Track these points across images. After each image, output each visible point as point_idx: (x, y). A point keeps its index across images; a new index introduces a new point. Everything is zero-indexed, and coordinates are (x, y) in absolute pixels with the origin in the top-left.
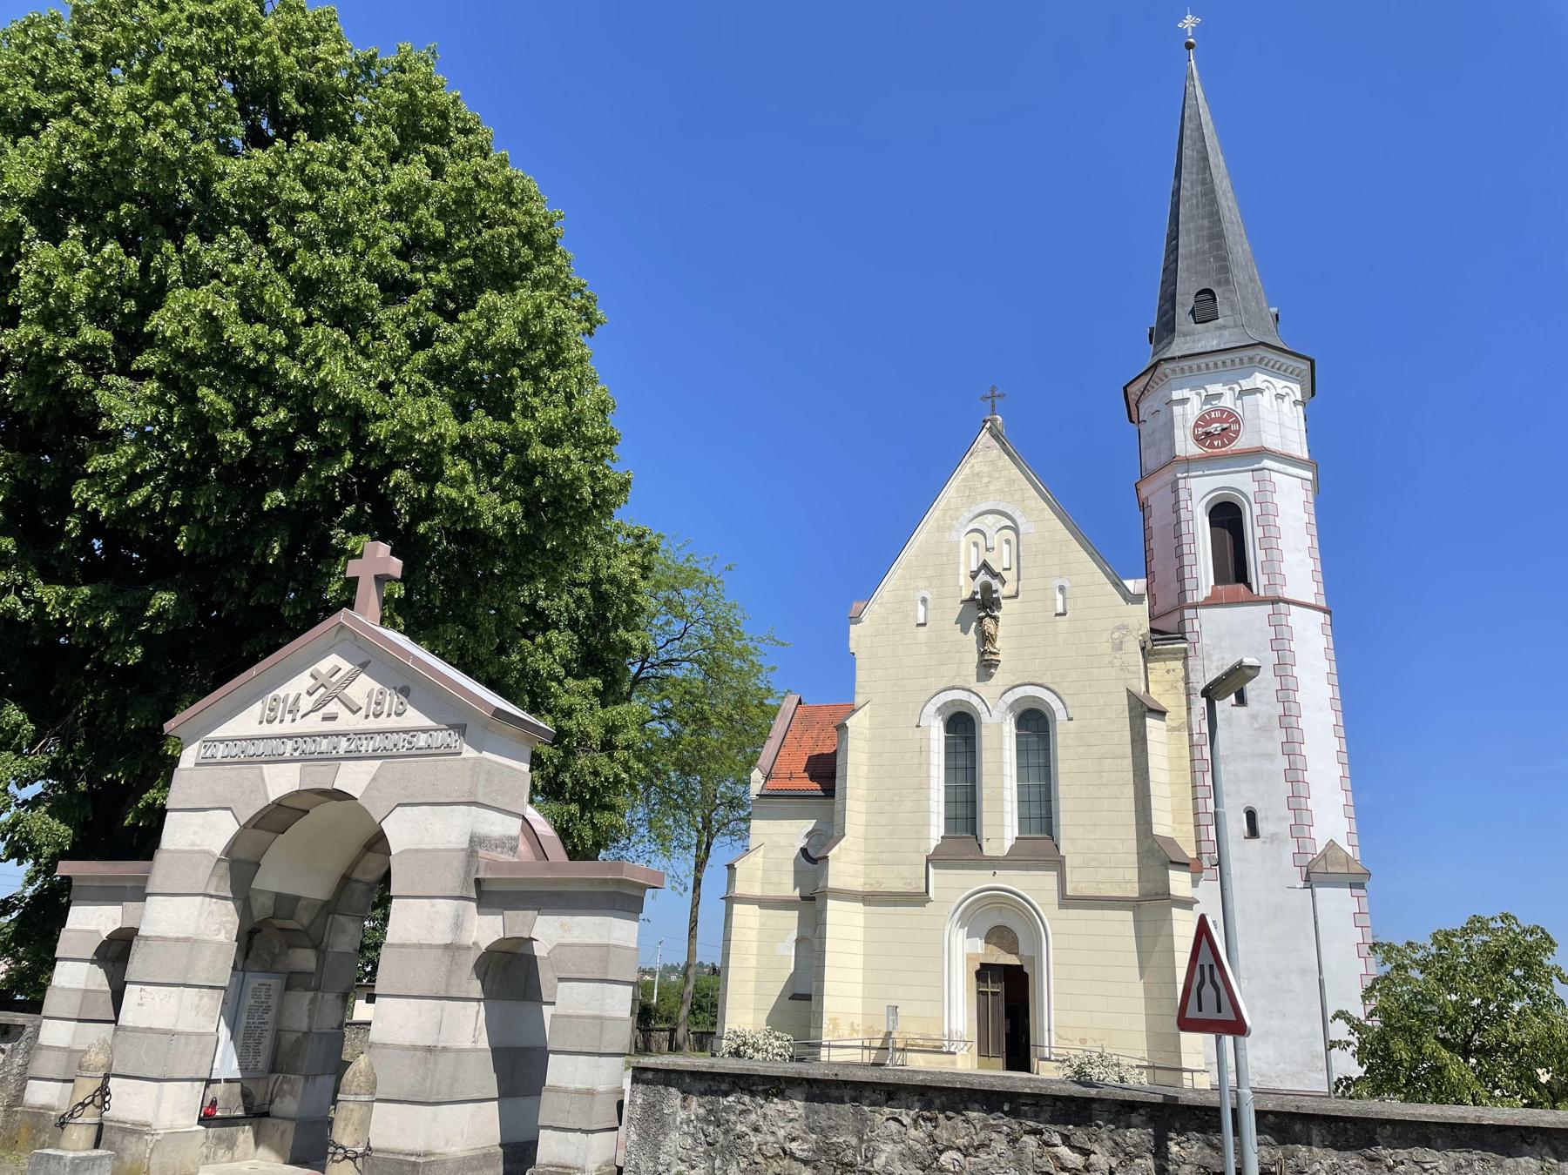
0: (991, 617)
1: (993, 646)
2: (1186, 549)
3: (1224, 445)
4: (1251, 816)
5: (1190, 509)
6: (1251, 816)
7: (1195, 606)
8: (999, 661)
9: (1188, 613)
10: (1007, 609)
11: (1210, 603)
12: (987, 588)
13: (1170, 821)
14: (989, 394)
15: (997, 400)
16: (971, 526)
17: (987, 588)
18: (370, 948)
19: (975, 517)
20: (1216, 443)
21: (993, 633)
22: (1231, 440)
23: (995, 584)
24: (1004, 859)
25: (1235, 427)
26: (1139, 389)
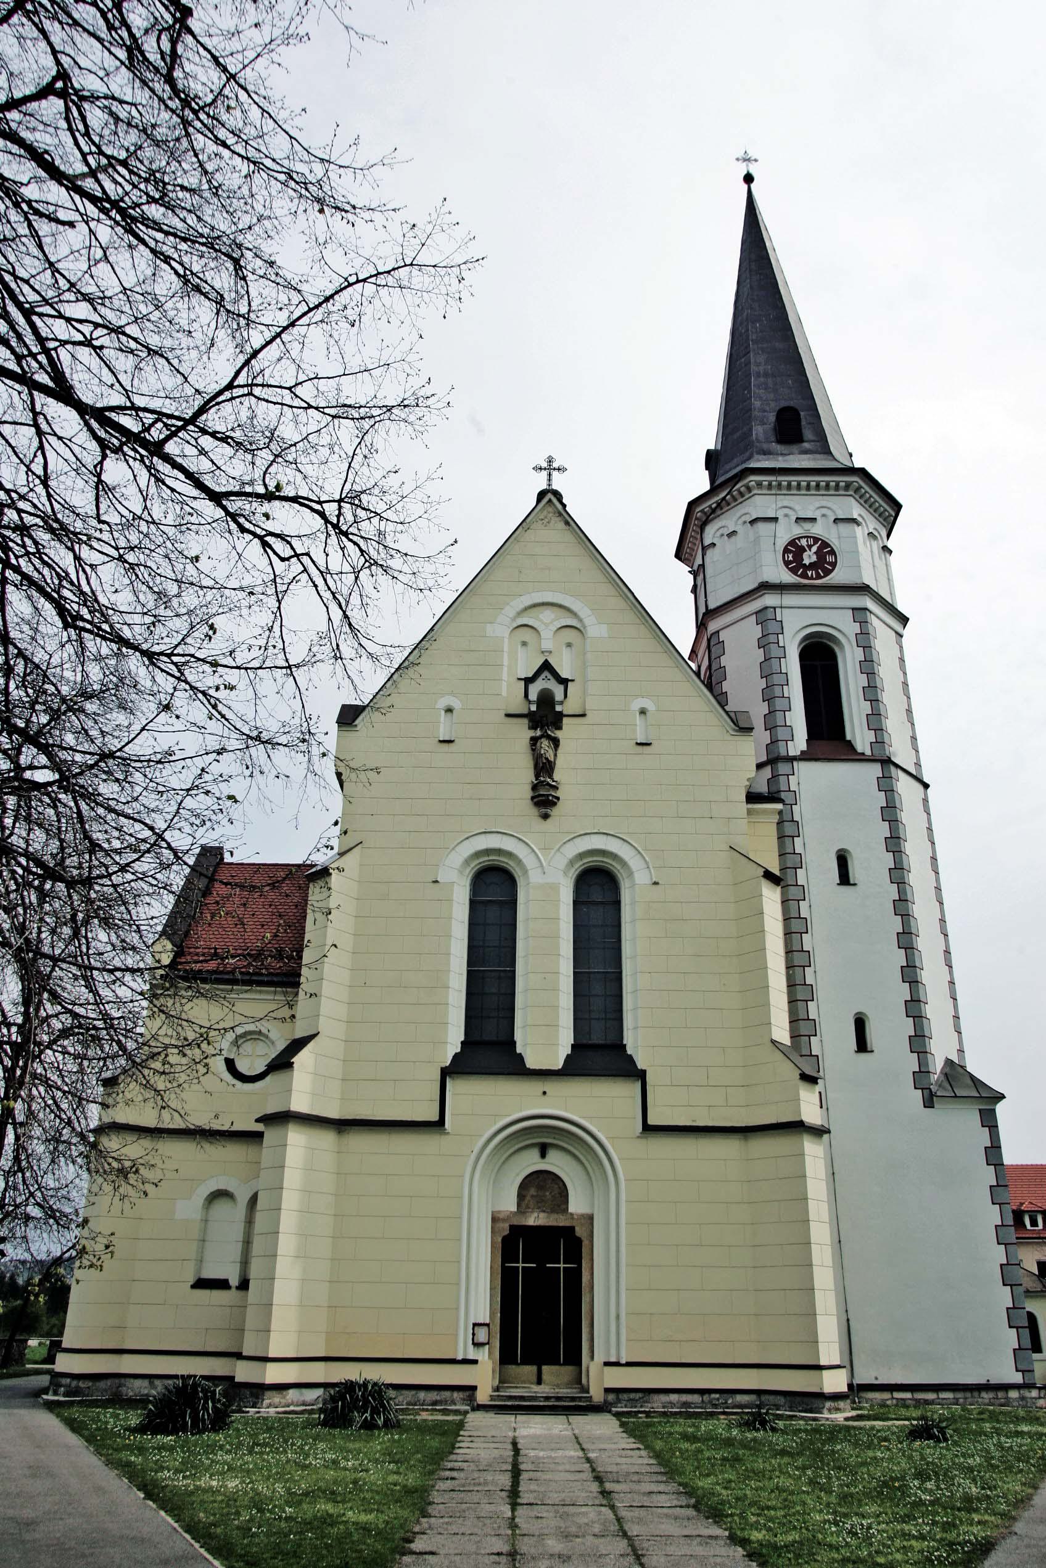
0: (549, 737)
1: (551, 777)
2: (777, 691)
3: (819, 577)
4: (842, 860)
5: (781, 644)
6: (842, 860)
7: (791, 759)
8: (558, 798)
9: (783, 768)
10: (568, 732)
11: (805, 757)
12: (546, 699)
13: (771, 898)
14: (545, 465)
15: (555, 474)
16: (520, 621)
17: (546, 699)
18: (750, 417)
19: (526, 609)
20: (809, 573)
21: (552, 759)
22: (828, 572)
23: (558, 691)
24: (559, 1070)
25: (830, 558)
26: (710, 506)
